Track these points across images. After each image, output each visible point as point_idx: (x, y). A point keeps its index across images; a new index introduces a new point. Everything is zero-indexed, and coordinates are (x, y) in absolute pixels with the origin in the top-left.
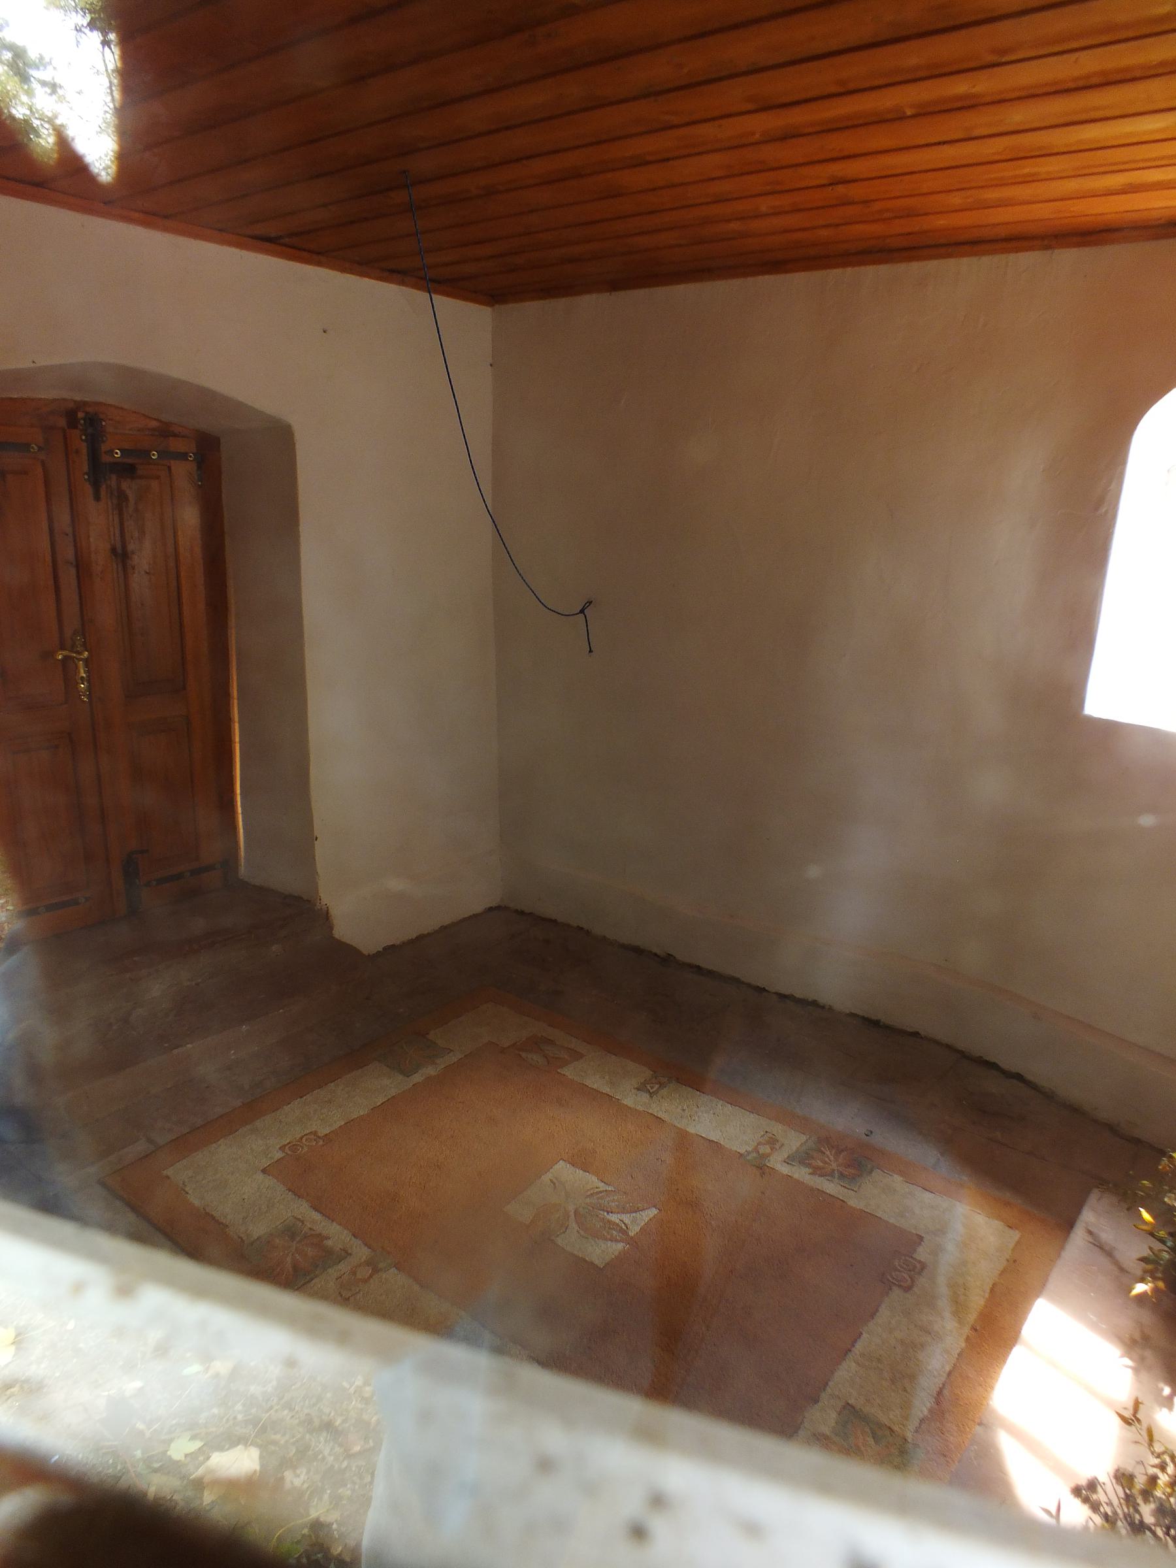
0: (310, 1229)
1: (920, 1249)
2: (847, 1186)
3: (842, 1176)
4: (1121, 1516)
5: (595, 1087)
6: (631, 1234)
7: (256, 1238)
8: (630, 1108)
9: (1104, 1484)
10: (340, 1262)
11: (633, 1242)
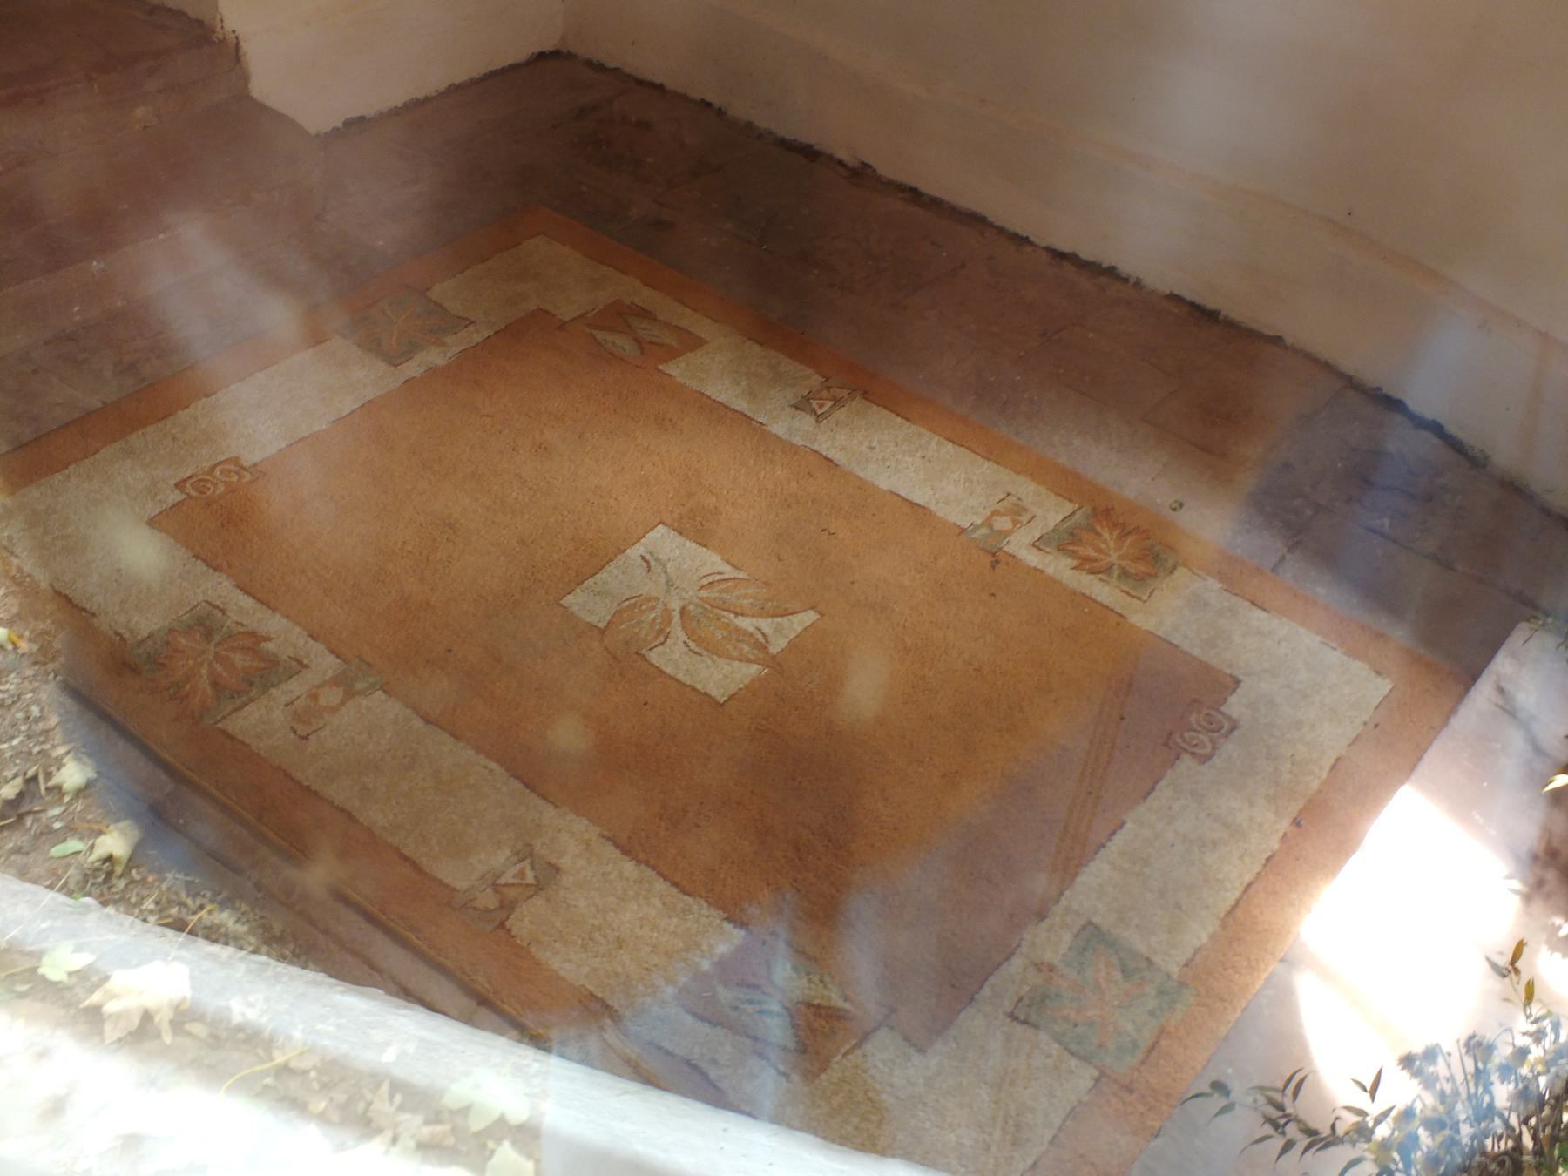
0: (237, 623)
1: (1232, 699)
2: (1132, 592)
3: (1125, 574)
4: (1464, 1096)
5: (722, 398)
6: (774, 650)
7: (146, 635)
8: (781, 440)
9: (1449, 1055)
10: (290, 678)
11: (776, 664)
